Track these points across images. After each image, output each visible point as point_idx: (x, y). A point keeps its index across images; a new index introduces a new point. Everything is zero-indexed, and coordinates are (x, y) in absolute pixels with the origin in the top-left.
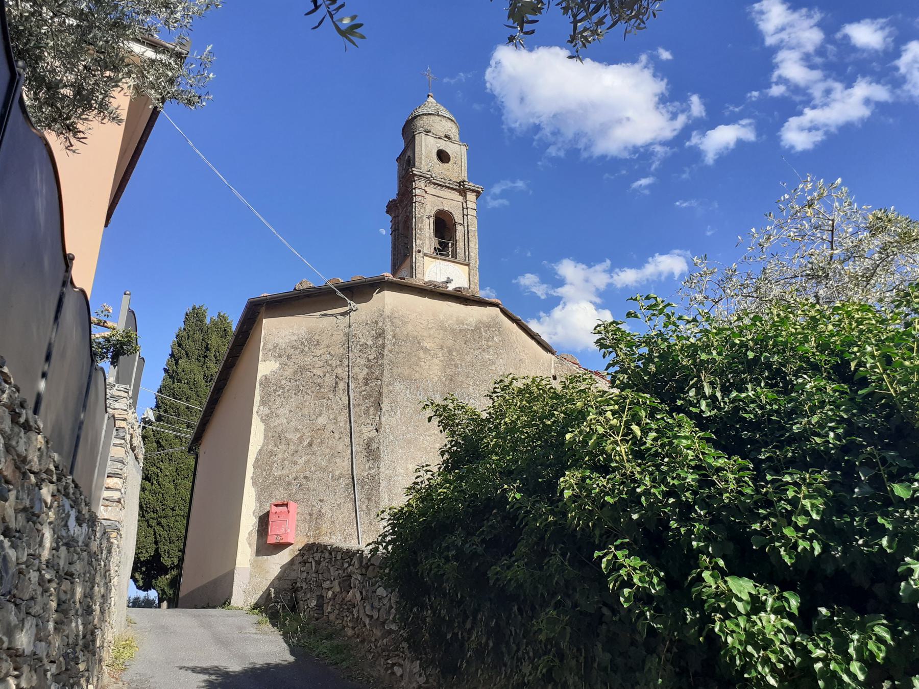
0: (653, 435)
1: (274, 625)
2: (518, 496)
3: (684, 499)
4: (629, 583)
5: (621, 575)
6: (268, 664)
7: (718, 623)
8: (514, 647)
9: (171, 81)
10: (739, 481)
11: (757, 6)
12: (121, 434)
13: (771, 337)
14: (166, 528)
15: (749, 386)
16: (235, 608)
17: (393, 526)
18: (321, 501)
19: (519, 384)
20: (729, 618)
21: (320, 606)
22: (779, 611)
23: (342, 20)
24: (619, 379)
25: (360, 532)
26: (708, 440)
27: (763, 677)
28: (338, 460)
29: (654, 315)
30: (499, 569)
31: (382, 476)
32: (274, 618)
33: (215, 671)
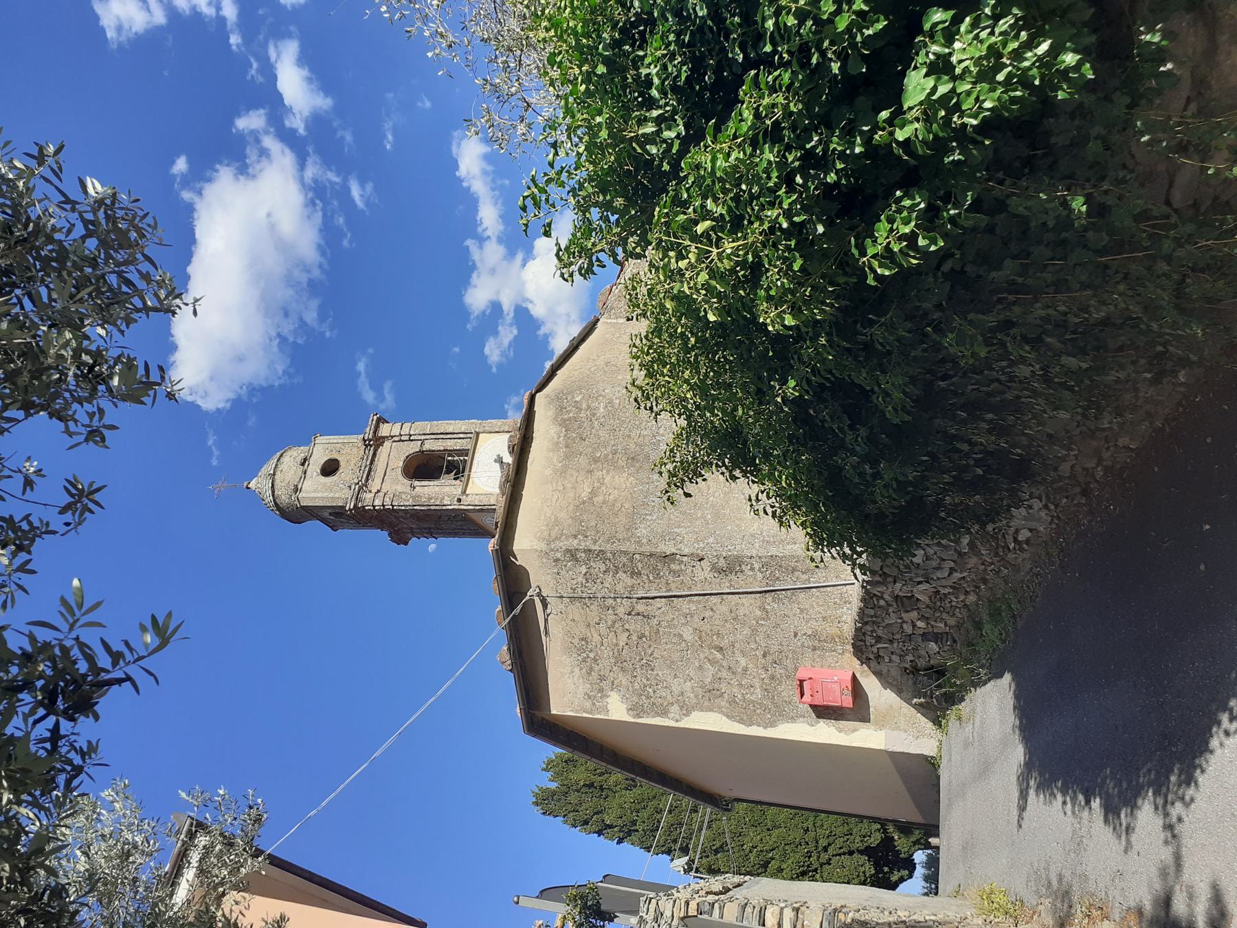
0: (710, 204)
1: (962, 700)
2: (792, 383)
3: (797, 164)
4: (911, 238)
5: (901, 250)
6: (1015, 708)
7: (966, 120)
8: (996, 385)
9: (230, 844)
10: (773, 89)
11: (110, 34)
12: (707, 907)
13: (578, 41)
14: (831, 839)
15: (644, 71)
16: (940, 750)
17: (831, 545)
18: (796, 635)
19: (640, 375)
20: (958, 105)
21: (937, 637)
22: (950, 36)
23: (146, 645)
24: (634, 248)
25: (839, 588)
26: (717, 129)
27: (1040, 59)
28: (741, 612)
29: (547, 200)
30: (890, 408)
31: (762, 553)
32: (952, 699)
33: (1023, 780)
